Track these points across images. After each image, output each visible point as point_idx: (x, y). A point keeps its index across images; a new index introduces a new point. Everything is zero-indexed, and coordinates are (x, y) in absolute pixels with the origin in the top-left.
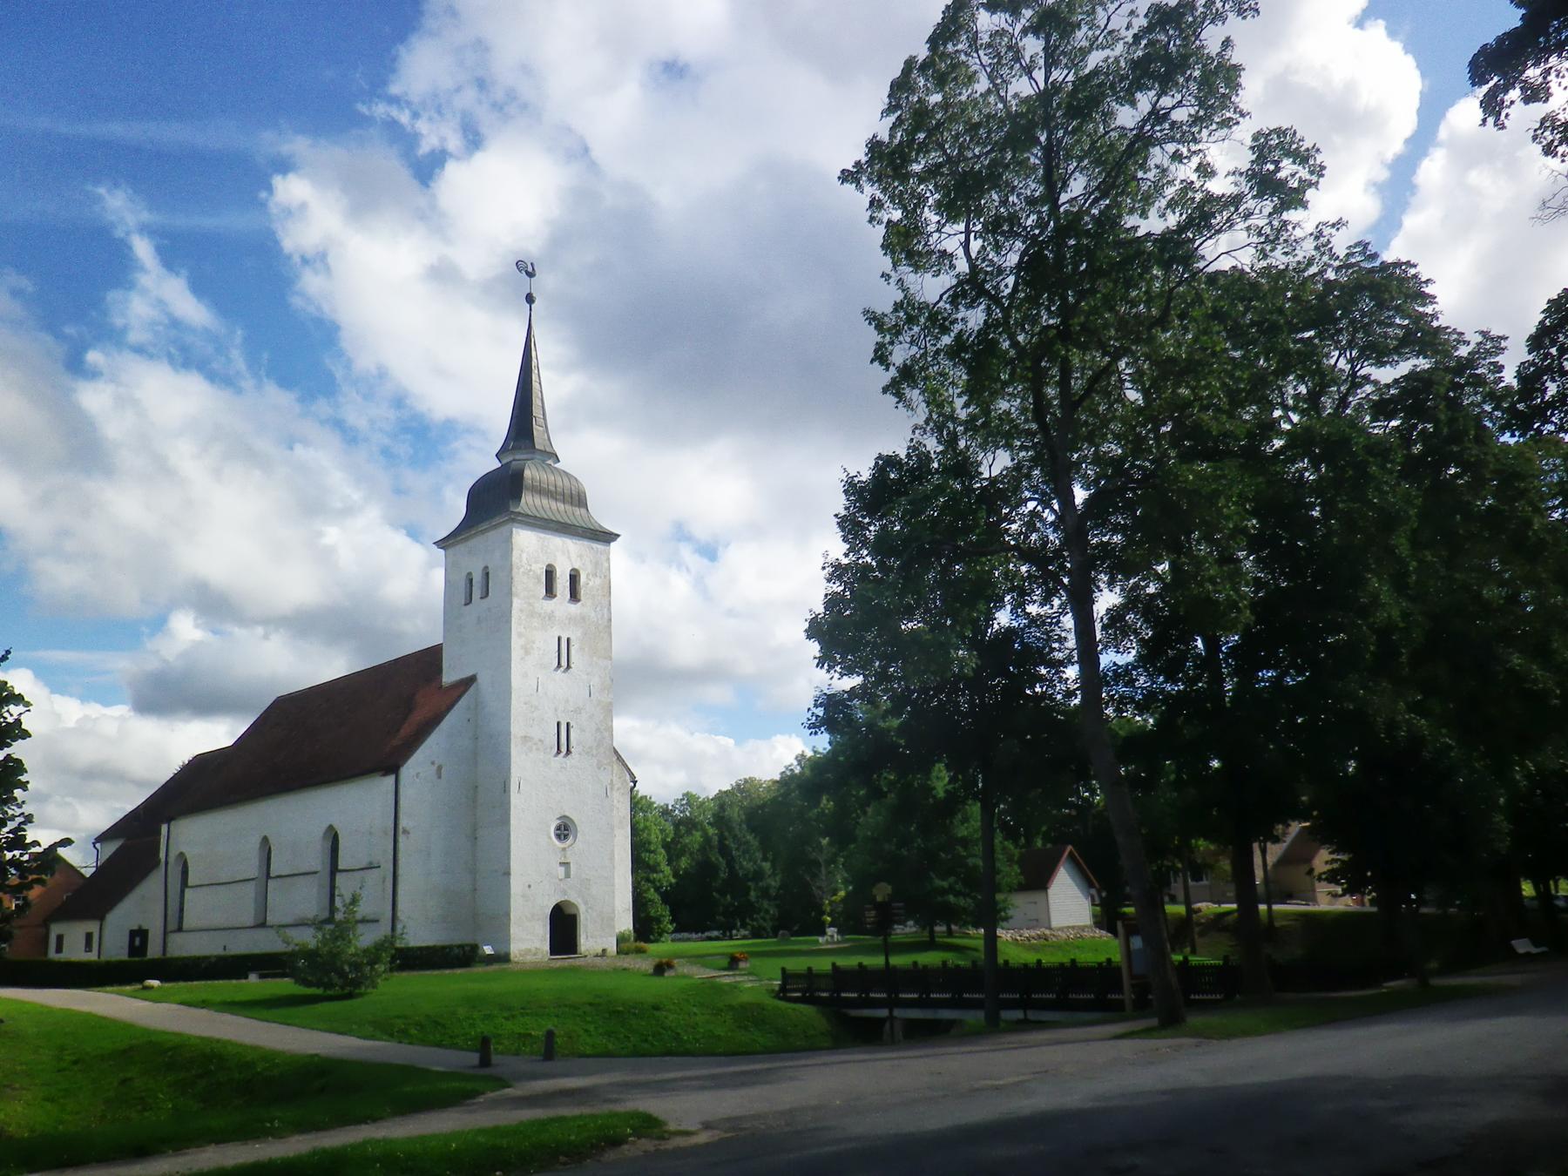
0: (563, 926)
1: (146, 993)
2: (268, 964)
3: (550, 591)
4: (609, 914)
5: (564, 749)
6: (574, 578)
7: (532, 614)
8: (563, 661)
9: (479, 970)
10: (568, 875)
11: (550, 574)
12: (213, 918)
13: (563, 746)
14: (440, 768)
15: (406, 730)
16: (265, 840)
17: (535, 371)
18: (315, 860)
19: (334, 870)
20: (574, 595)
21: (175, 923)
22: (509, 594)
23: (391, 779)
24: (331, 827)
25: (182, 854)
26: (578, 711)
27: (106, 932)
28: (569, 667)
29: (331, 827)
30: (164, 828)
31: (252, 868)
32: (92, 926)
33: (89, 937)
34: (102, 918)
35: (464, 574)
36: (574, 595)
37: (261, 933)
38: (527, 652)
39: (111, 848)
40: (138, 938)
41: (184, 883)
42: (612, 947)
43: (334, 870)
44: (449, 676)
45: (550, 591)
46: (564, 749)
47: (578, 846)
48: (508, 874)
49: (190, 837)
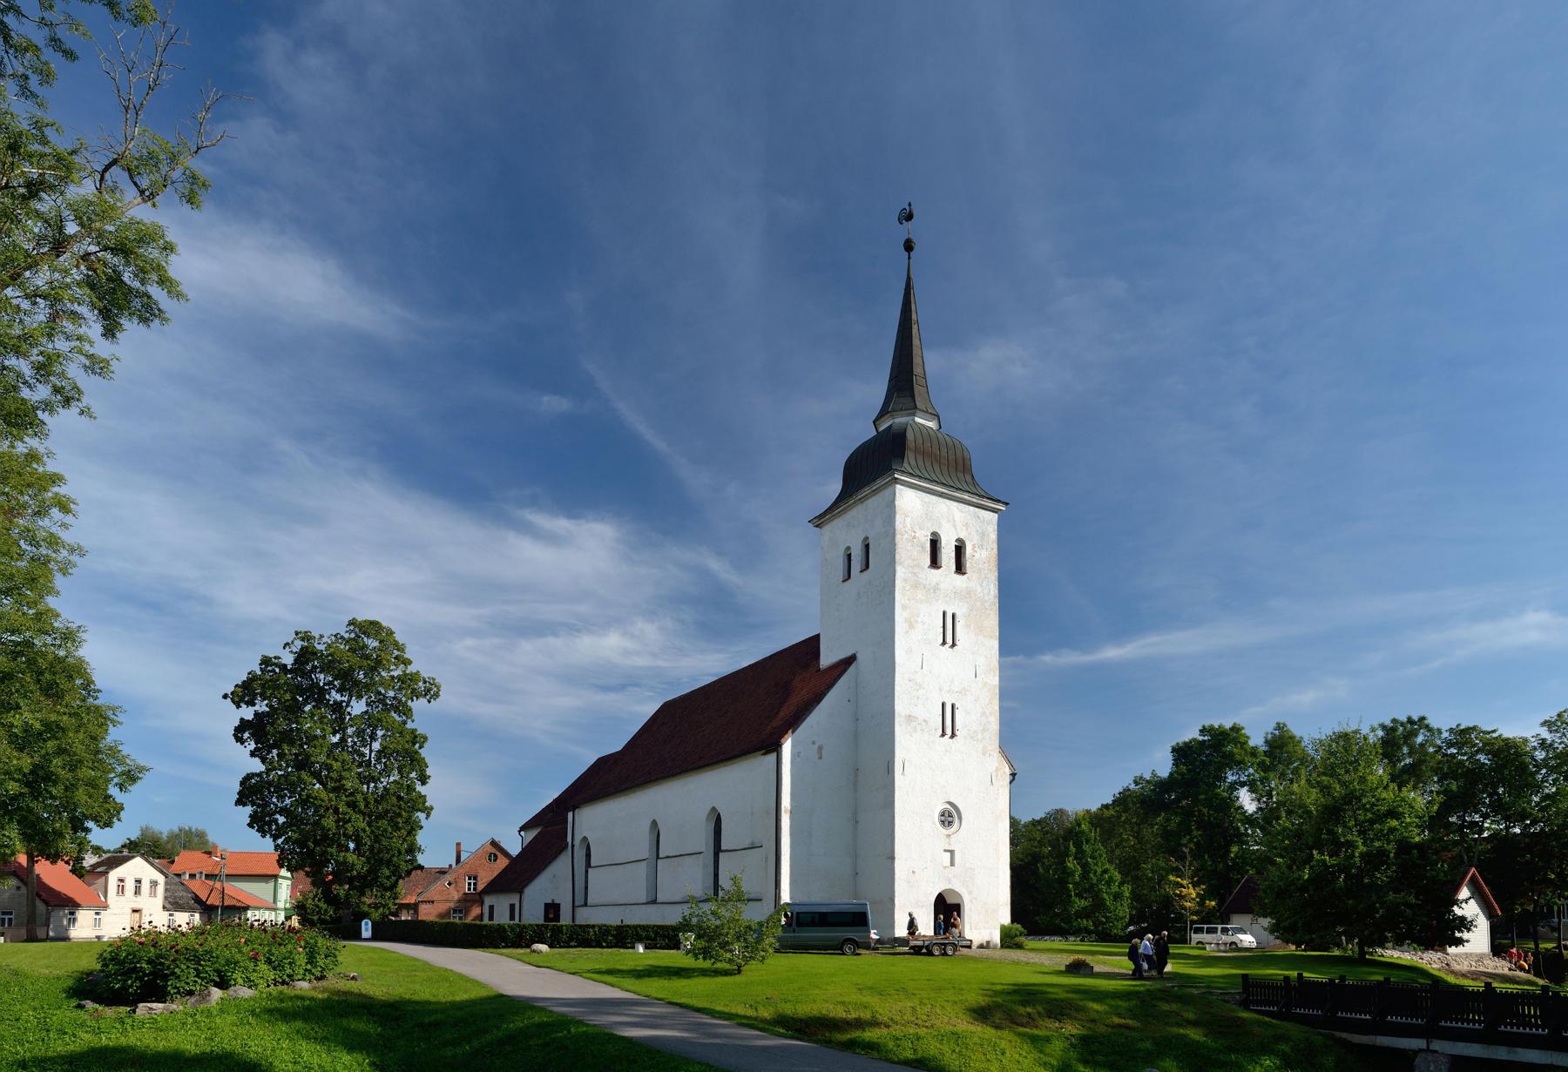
0: (912, 926)
1: (534, 958)
2: (664, 937)
3: (935, 562)
4: (988, 913)
5: (949, 731)
6: (960, 550)
7: (916, 586)
8: (949, 638)
9: (866, 957)
10: (952, 864)
11: (935, 544)
12: (614, 895)
13: (949, 729)
14: (820, 748)
15: (785, 712)
16: (654, 823)
17: (915, 327)
18: (701, 839)
19: (718, 849)
20: (960, 568)
21: (582, 899)
22: (892, 563)
23: (773, 756)
24: (714, 809)
25: (585, 838)
26: (963, 692)
27: (525, 904)
28: (954, 645)
29: (714, 809)
30: (570, 815)
31: (644, 850)
32: (515, 899)
33: (512, 907)
34: (521, 893)
35: (842, 549)
36: (960, 568)
37: (653, 908)
38: (911, 626)
39: (532, 834)
40: (552, 909)
41: (588, 865)
42: (997, 939)
43: (718, 849)
44: (827, 659)
45: (935, 562)
46: (949, 731)
47: (962, 837)
48: (892, 858)
49: (590, 822)
